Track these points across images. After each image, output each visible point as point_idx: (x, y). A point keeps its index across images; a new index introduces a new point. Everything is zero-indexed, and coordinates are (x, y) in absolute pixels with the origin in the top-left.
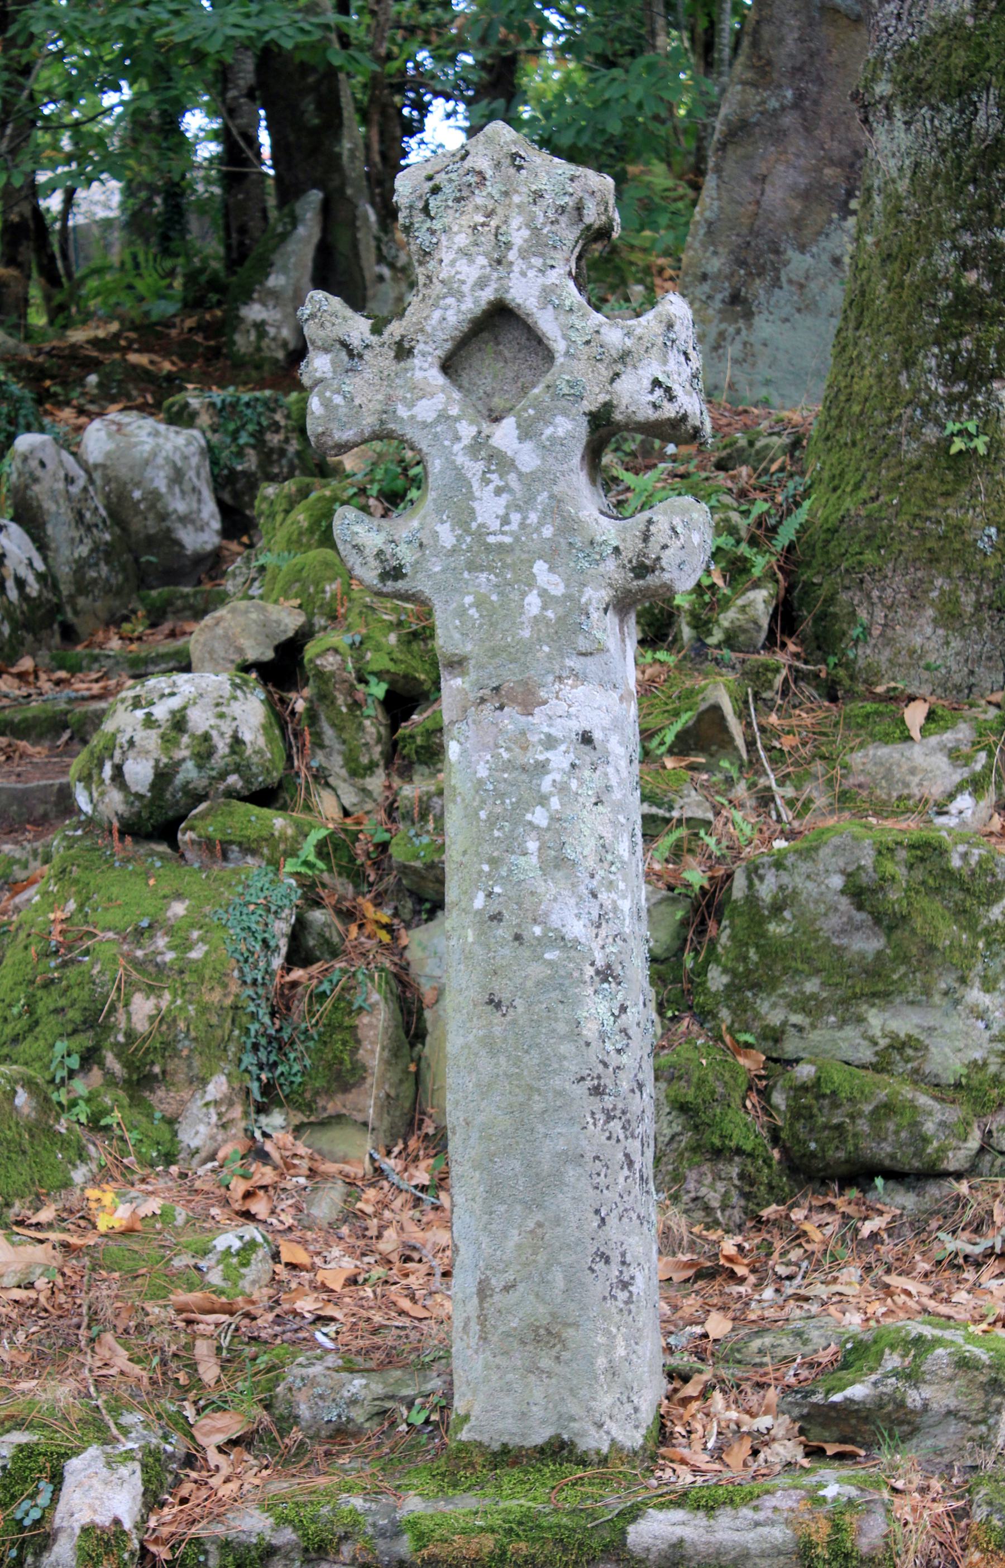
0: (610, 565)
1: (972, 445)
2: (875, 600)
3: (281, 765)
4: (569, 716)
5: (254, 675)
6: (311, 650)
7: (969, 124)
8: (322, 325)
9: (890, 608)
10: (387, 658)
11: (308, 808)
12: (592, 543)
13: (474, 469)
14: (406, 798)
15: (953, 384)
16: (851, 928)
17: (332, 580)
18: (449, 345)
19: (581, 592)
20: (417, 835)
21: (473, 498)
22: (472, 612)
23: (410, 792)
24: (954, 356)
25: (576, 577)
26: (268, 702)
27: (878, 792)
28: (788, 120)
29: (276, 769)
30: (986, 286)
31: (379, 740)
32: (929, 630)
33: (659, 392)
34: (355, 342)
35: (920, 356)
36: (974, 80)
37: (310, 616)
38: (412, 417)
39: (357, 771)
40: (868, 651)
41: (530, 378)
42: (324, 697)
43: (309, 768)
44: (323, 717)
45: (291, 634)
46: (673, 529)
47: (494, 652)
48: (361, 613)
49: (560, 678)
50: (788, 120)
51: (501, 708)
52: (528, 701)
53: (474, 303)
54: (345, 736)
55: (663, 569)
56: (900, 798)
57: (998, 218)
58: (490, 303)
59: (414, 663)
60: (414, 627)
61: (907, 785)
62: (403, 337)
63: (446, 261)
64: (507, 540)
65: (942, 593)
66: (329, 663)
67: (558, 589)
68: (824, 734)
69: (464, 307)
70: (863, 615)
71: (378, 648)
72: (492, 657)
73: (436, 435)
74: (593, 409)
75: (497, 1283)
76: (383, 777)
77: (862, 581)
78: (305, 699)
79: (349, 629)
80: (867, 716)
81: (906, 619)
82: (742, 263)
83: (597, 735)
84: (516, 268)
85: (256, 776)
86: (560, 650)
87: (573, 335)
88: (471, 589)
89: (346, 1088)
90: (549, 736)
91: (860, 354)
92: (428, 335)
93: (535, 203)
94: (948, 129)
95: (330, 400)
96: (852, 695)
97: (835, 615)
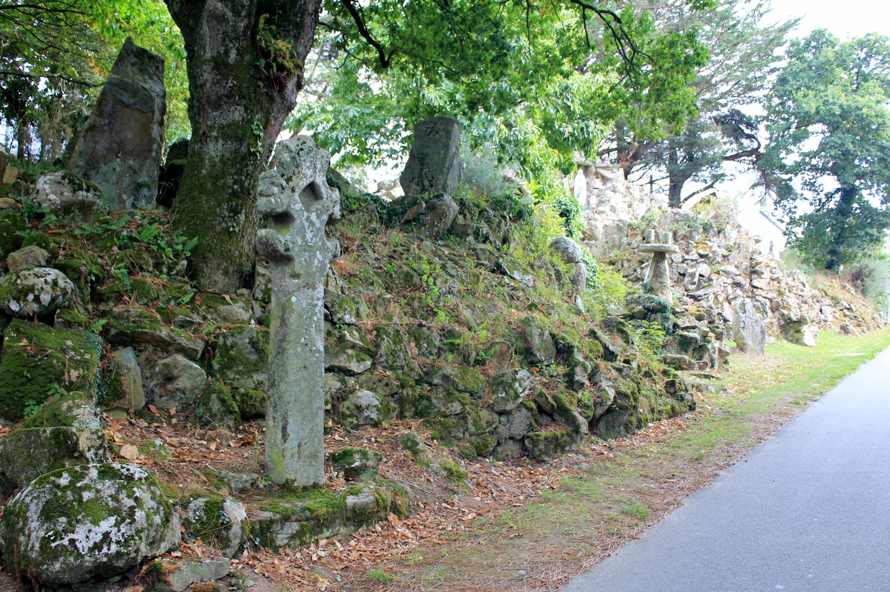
16: (250, 353)
28: (106, 128)
47: (308, 274)
50: (106, 128)
67: (321, 259)
70: (205, 270)
75: (303, 443)
82: (88, 165)
89: (119, 399)
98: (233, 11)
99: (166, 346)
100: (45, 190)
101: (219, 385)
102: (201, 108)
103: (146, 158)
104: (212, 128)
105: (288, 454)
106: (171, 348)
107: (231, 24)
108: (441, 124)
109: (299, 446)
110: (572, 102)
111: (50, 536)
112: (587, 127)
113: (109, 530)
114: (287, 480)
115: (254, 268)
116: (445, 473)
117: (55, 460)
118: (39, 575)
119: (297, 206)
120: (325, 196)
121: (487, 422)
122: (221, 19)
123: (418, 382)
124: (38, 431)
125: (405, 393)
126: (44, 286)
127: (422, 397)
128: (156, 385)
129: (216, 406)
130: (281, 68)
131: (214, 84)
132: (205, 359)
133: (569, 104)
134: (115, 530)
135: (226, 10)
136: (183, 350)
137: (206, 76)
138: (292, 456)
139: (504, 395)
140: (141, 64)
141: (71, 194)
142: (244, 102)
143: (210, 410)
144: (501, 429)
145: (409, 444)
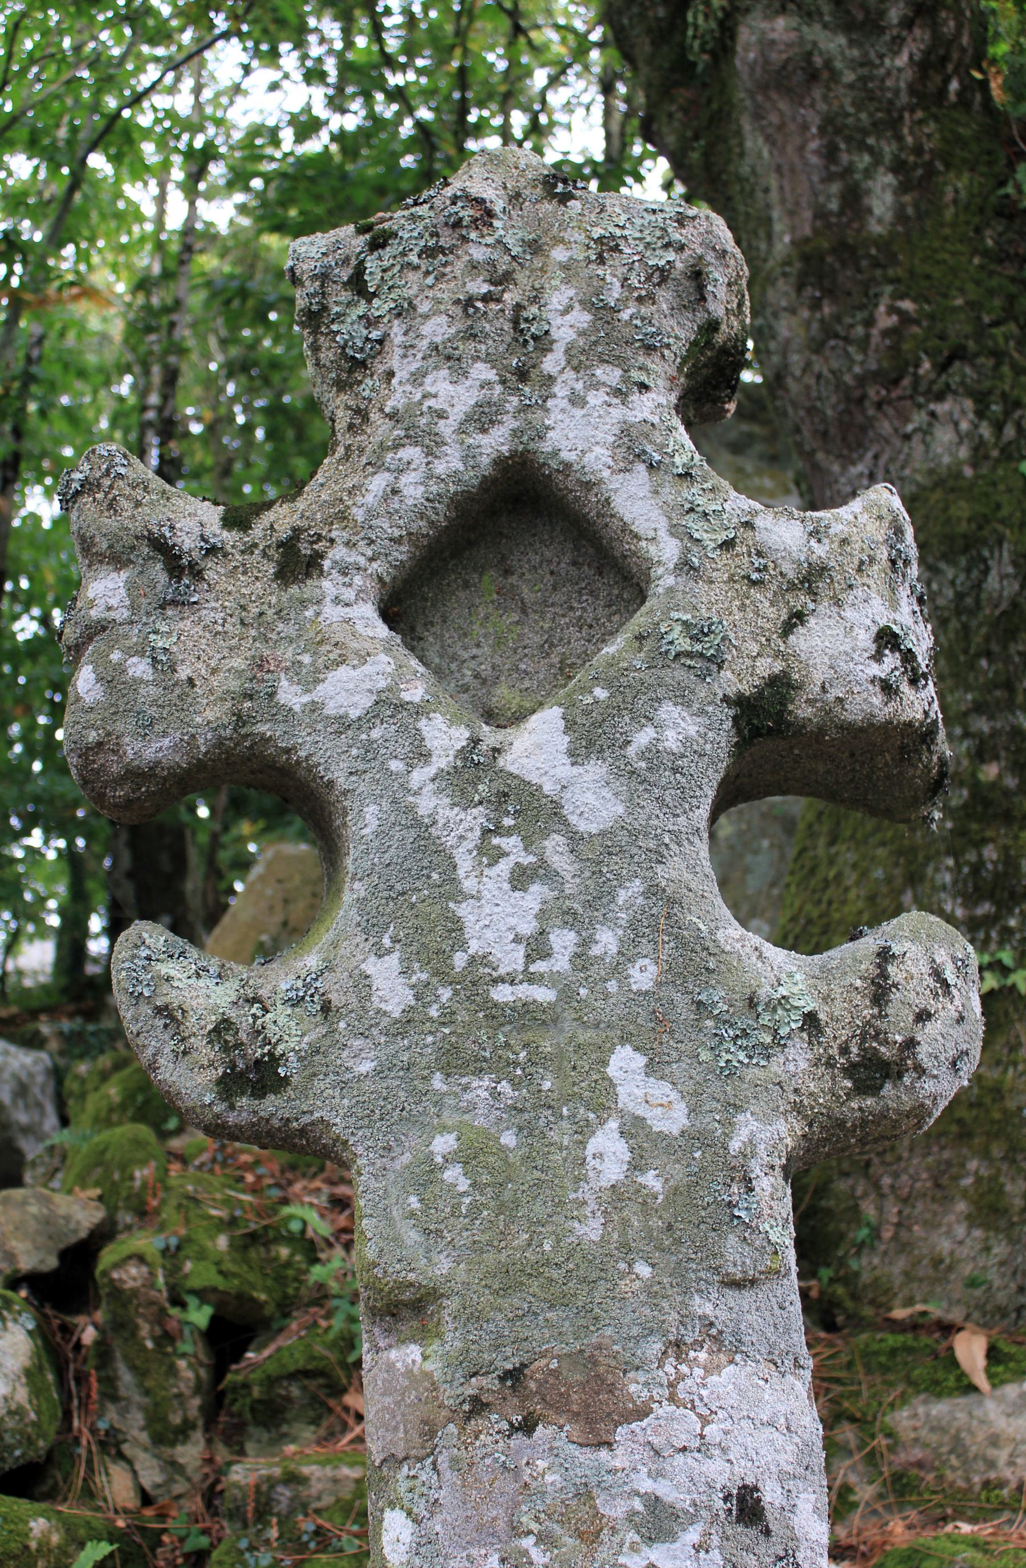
0: (797, 1059)
1: (1009, 982)
2: (886, 1190)
3: (51, 1429)
4: (704, 1448)
5: (24, 1293)
6: (108, 1256)
7: (978, 586)
8: (112, 505)
9: (905, 1200)
10: (213, 1269)
11: (89, 1493)
12: (752, 1002)
13: (460, 825)
14: (236, 1485)
15: (976, 904)
17: (143, 1163)
18: (401, 554)
19: (729, 1124)
20: (252, 1548)
21: (460, 896)
22: (453, 1174)
23: (243, 1474)
24: (977, 868)
25: (715, 1087)
26: (42, 1334)
27: (949, 1475)
29: (44, 1436)
30: (1011, 782)
31: (198, 1389)
32: (960, 1231)
33: (891, 660)
34: (187, 542)
35: (930, 871)
36: (985, 533)
37: (112, 1212)
38: (314, 707)
39: (165, 1435)
40: (876, 1261)
41: (578, 646)
42: (121, 1326)
43: (94, 1431)
44: (118, 1355)
45: (83, 1234)
46: (937, 974)
47: (508, 1280)
48: (179, 1206)
49: (678, 1347)
51: (527, 1427)
52: (599, 1411)
53: (463, 458)
54: (149, 1383)
55: (920, 1070)
56: (986, 1484)
57: (1020, 698)
58: (500, 462)
59: (251, 1277)
60: (253, 1226)
61: (991, 1464)
62: (297, 531)
63: (401, 375)
64: (544, 995)
65: (979, 1180)
66: (132, 1276)
67: (671, 1118)
68: (838, 1381)
69: (440, 468)
70: (869, 1210)
71: (201, 1256)
72: (504, 1291)
73: (369, 747)
74: (746, 688)
76: (202, 1443)
77: (868, 1164)
78: (96, 1326)
79: (162, 1227)
80: (893, 1352)
81: (928, 1216)
83: (771, 1495)
84: (560, 390)
85: (11, 1448)
86: (679, 1271)
87: (698, 529)
88: (449, 1118)
90: (654, 1502)
91: (839, 876)
92: (357, 528)
93: (601, 260)
94: (950, 593)
95: (121, 668)
96: (858, 1323)
97: (829, 1212)
98: (848, 26)
107: (849, 77)
119: (346, 674)
120: (667, 550)
135: (815, 33)
140: (773, 437)
142: (962, 372)
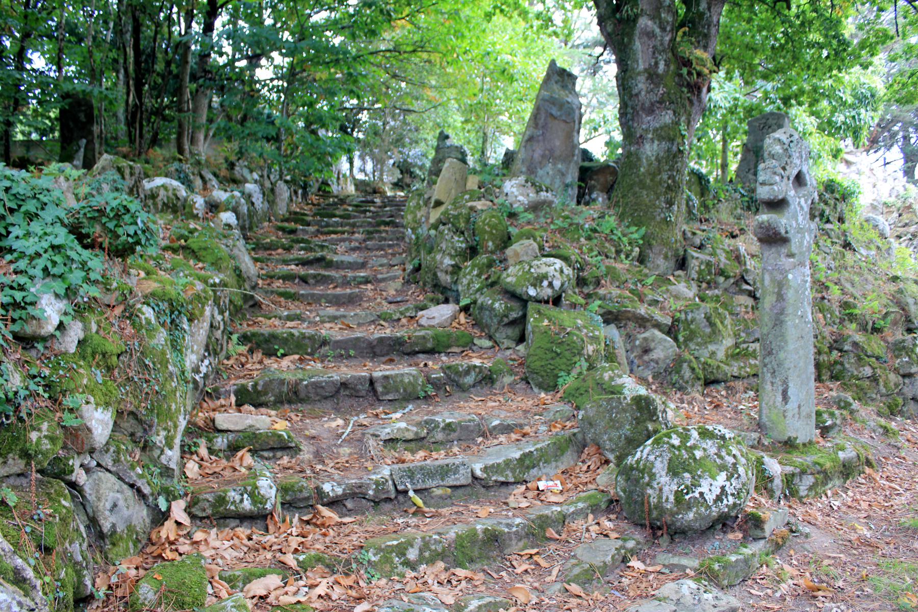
16: (706, 326)
47: (800, 253)
50: (541, 138)
98: (660, 27)
99: (643, 322)
100: (513, 192)
101: (687, 356)
102: (636, 113)
103: (570, 162)
104: (647, 131)
105: (789, 414)
106: (648, 324)
108: (773, 119)
109: (799, 407)
110: (844, 93)
111: (682, 490)
112: (859, 115)
113: (724, 484)
114: (790, 438)
115: (685, 251)
116: (881, 431)
117: (638, 423)
118: (673, 523)
121: (895, 384)
122: (650, 35)
123: (831, 348)
124: (619, 398)
125: (821, 359)
126: (556, 274)
127: (836, 362)
128: (635, 357)
129: (687, 374)
130: (699, 74)
131: (648, 92)
132: (671, 331)
133: (841, 95)
134: (728, 484)
136: (658, 326)
137: (640, 86)
138: (793, 416)
139: (907, 359)
141: (535, 195)
142: (673, 106)
143: (682, 377)
144: (905, 390)
145: (842, 404)
